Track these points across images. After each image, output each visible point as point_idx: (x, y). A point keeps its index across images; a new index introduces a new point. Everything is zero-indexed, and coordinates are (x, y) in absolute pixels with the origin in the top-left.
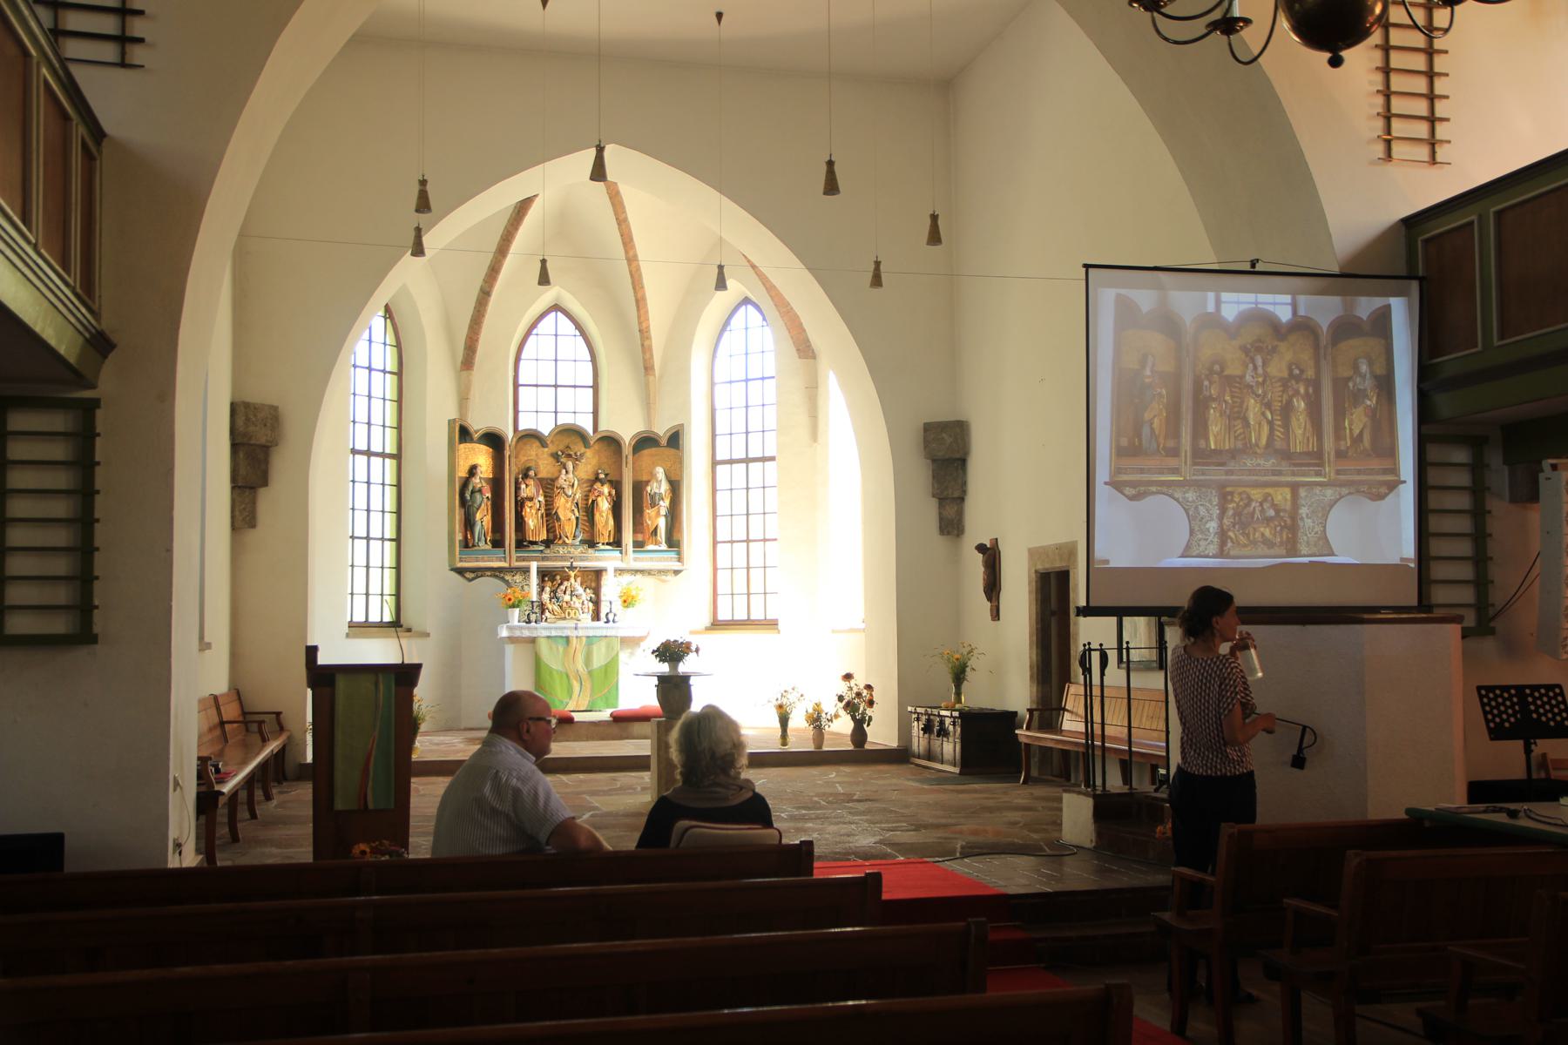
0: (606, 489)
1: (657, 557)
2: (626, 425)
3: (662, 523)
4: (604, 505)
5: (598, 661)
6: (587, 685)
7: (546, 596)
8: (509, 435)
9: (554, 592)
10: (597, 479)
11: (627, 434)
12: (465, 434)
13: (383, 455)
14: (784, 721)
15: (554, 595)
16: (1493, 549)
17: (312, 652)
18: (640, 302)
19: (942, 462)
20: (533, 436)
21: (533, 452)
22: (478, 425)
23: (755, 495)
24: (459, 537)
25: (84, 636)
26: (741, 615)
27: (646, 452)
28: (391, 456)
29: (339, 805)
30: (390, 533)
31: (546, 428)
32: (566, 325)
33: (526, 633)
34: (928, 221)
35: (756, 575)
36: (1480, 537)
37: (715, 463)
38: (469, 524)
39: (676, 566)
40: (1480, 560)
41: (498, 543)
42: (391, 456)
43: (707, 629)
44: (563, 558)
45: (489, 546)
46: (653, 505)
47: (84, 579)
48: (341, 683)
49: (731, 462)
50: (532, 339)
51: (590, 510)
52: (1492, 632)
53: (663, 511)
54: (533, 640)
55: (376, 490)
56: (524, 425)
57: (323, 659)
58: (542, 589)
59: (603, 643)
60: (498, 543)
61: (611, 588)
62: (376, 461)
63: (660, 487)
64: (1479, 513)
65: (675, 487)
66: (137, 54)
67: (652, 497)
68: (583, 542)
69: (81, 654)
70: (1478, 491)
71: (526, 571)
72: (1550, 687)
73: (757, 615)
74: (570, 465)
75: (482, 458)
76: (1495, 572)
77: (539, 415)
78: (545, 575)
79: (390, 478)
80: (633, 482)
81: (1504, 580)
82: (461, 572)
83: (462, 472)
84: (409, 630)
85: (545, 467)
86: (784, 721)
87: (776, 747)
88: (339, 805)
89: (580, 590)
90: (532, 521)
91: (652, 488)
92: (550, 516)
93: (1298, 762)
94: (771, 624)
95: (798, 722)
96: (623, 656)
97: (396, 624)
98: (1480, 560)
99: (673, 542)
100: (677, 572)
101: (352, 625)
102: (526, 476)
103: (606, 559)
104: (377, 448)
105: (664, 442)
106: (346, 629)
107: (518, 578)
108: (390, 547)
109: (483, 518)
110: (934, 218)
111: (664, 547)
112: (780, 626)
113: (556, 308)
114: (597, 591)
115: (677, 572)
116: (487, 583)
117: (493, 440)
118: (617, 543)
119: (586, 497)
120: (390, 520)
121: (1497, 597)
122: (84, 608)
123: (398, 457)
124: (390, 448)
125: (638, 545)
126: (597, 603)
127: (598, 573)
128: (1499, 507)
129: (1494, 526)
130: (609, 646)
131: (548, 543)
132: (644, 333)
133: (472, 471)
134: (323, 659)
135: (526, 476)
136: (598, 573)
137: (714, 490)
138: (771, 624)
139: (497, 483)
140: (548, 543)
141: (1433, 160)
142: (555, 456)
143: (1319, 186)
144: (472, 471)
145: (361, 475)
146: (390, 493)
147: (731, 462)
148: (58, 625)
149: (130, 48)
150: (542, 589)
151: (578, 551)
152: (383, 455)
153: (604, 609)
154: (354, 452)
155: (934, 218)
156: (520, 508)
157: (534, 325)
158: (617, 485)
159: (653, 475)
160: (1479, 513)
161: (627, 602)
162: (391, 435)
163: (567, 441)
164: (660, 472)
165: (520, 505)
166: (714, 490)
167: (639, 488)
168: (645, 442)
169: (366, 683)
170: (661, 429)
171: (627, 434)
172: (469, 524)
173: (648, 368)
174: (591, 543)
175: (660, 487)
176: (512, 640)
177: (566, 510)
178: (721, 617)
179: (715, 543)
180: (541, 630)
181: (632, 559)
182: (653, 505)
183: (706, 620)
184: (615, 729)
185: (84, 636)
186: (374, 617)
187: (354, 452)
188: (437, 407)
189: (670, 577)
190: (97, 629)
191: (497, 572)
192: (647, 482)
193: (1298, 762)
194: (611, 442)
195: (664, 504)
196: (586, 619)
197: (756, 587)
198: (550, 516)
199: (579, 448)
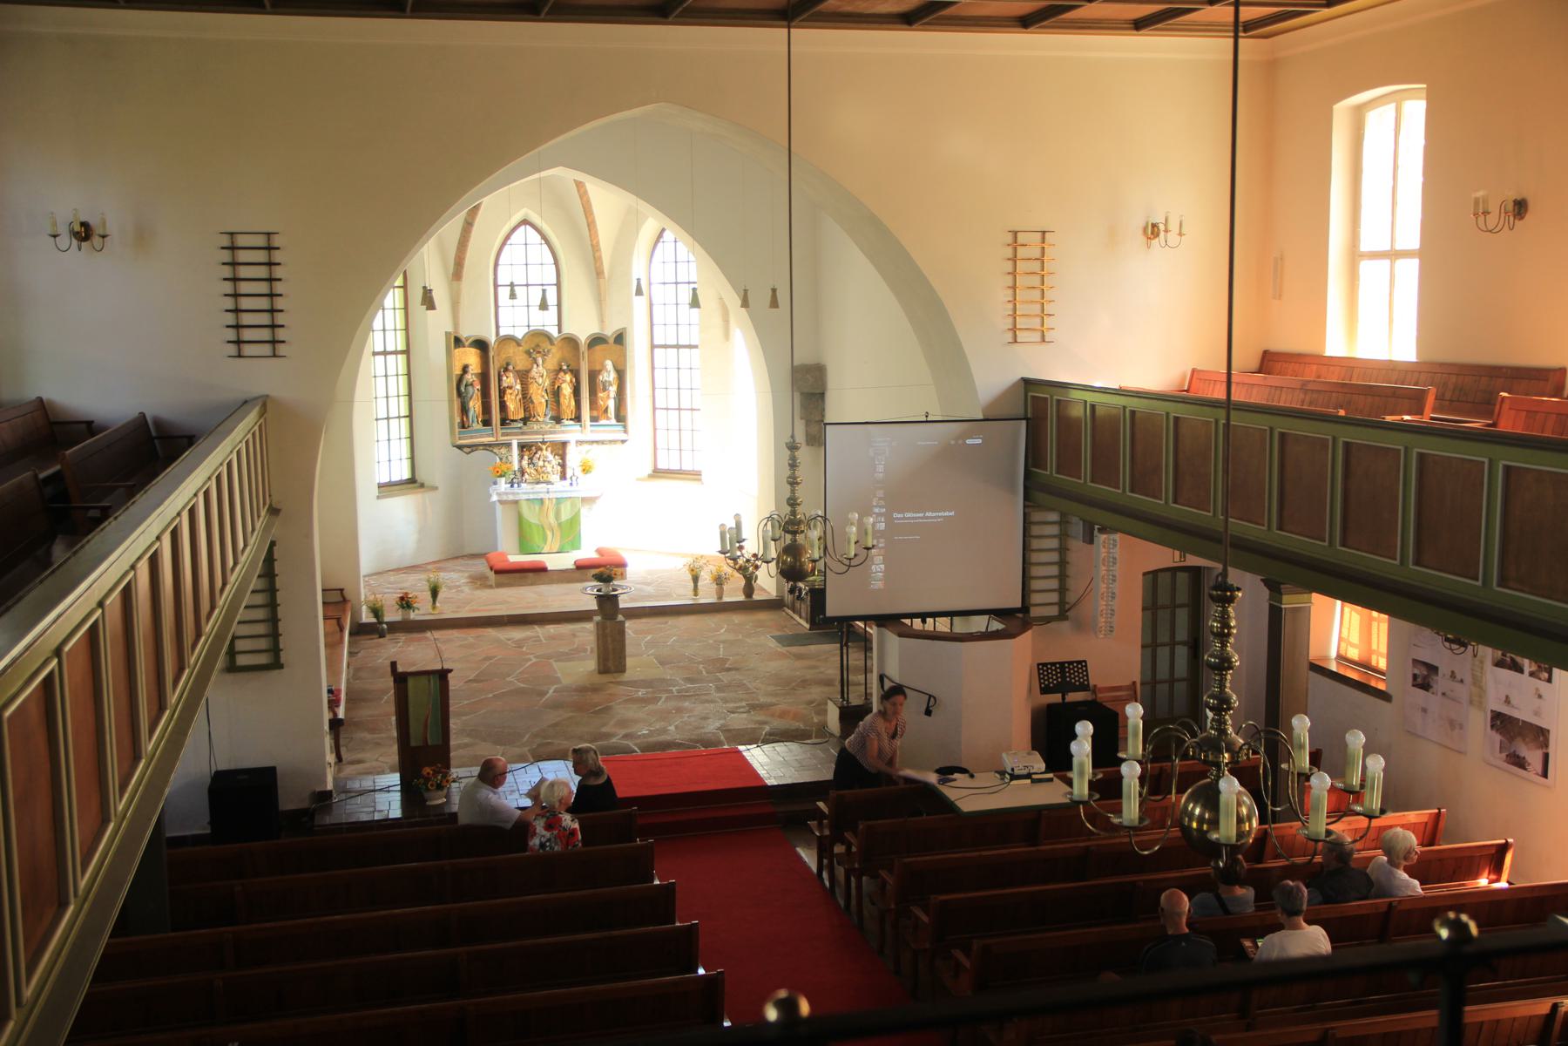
0: (568, 377)
1: (608, 429)
2: (582, 327)
3: (611, 404)
4: (567, 390)
5: (565, 515)
6: (557, 533)
7: (525, 463)
8: (492, 339)
9: (531, 459)
10: (561, 369)
11: (583, 338)
12: (458, 342)
13: (396, 353)
14: (695, 579)
15: (531, 462)
16: (1071, 571)
17: (394, 664)
18: (591, 225)
19: (807, 392)
20: (510, 339)
21: (511, 350)
22: (468, 332)
23: (684, 374)
24: (458, 420)
25: (276, 665)
26: (675, 466)
27: (598, 348)
28: (402, 352)
29: (413, 743)
30: (404, 411)
31: (519, 333)
32: (534, 236)
33: (511, 498)
34: (770, 293)
35: (686, 435)
36: (1063, 564)
37: (653, 347)
38: (464, 410)
39: (623, 436)
40: (1062, 577)
41: (487, 423)
42: (402, 352)
43: (650, 476)
44: (537, 433)
45: (480, 426)
46: (605, 389)
47: (274, 635)
48: (411, 682)
49: (666, 346)
50: (507, 248)
51: (556, 393)
52: (1066, 618)
53: (612, 394)
54: (516, 502)
55: (392, 380)
56: (503, 332)
57: (400, 669)
58: (522, 457)
59: (568, 503)
60: (487, 423)
61: (574, 456)
62: (391, 358)
63: (609, 375)
64: (1063, 550)
65: (621, 374)
66: (281, 349)
67: (604, 383)
68: (552, 418)
69: (275, 673)
70: (1063, 536)
71: (509, 445)
72: (1079, 662)
73: (687, 467)
74: (540, 361)
75: (472, 358)
76: (1071, 583)
77: (516, 320)
78: (523, 447)
79: (402, 369)
80: (587, 373)
81: (1076, 586)
82: (460, 447)
83: (458, 371)
84: (422, 486)
85: (521, 362)
86: (695, 579)
87: (687, 600)
88: (413, 743)
89: (551, 457)
90: (513, 404)
91: (604, 377)
92: (525, 397)
93: (928, 712)
94: (695, 475)
95: (706, 579)
96: (584, 511)
97: (412, 480)
98: (1062, 577)
99: (620, 417)
100: (623, 442)
101: (381, 486)
102: (506, 370)
103: (570, 433)
104: (390, 348)
105: (611, 341)
106: (376, 491)
107: (503, 450)
108: (405, 422)
109: (475, 405)
110: (774, 291)
111: (613, 421)
112: (703, 477)
113: (525, 222)
114: (563, 457)
115: (623, 442)
116: (480, 453)
117: (481, 345)
118: (577, 418)
119: (553, 384)
120: (404, 401)
121: (1071, 597)
122: (275, 650)
123: (407, 352)
124: (401, 347)
125: (594, 419)
126: (563, 466)
127: (564, 444)
128: (1076, 545)
129: (1072, 557)
130: (573, 505)
131: (525, 420)
132: (595, 248)
133: (465, 369)
134: (400, 669)
135: (506, 370)
136: (564, 444)
137: (653, 368)
138: (695, 475)
139: (484, 377)
140: (525, 420)
141: (1044, 340)
142: (528, 353)
143: (969, 357)
144: (465, 369)
145: (380, 371)
146: (403, 380)
147: (666, 346)
148: (263, 659)
149: (279, 346)
150: (522, 457)
151: (549, 425)
152: (396, 353)
153: (569, 473)
154: (375, 354)
155: (774, 291)
156: (502, 398)
157: (508, 237)
158: (576, 374)
159: (603, 367)
160: (1063, 550)
161: (586, 469)
162: (401, 336)
163: (537, 340)
164: (609, 364)
165: (502, 393)
166: (653, 368)
167: (593, 376)
168: (597, 341)
169: (423, 680)
170: (609, 332)
171: (583, 338)
172: (464, 410)
173: (599, 273)
174: (558, 419)
175: (609, 375)
176: (500, 502)
177: (540, 398)
178: (660, 466)
179: (654, 409)
180: (525, 491)
181: (587, 431)
182: (605, 389)
183: (649, 470)
184: (578, 574)
185: (276, 665)
186: (396, 478)
187: (375, 354)
188: (437, 325)
189: (619, 445)
190: (282, 660)
191: (487, 447)
192: (599, 372)
193: (928, 712)
194: (571, 341)
195: (613, 389)
196: (555, 478)
197: (686, 444)
198: (525, 397)
199: (546, 346)
